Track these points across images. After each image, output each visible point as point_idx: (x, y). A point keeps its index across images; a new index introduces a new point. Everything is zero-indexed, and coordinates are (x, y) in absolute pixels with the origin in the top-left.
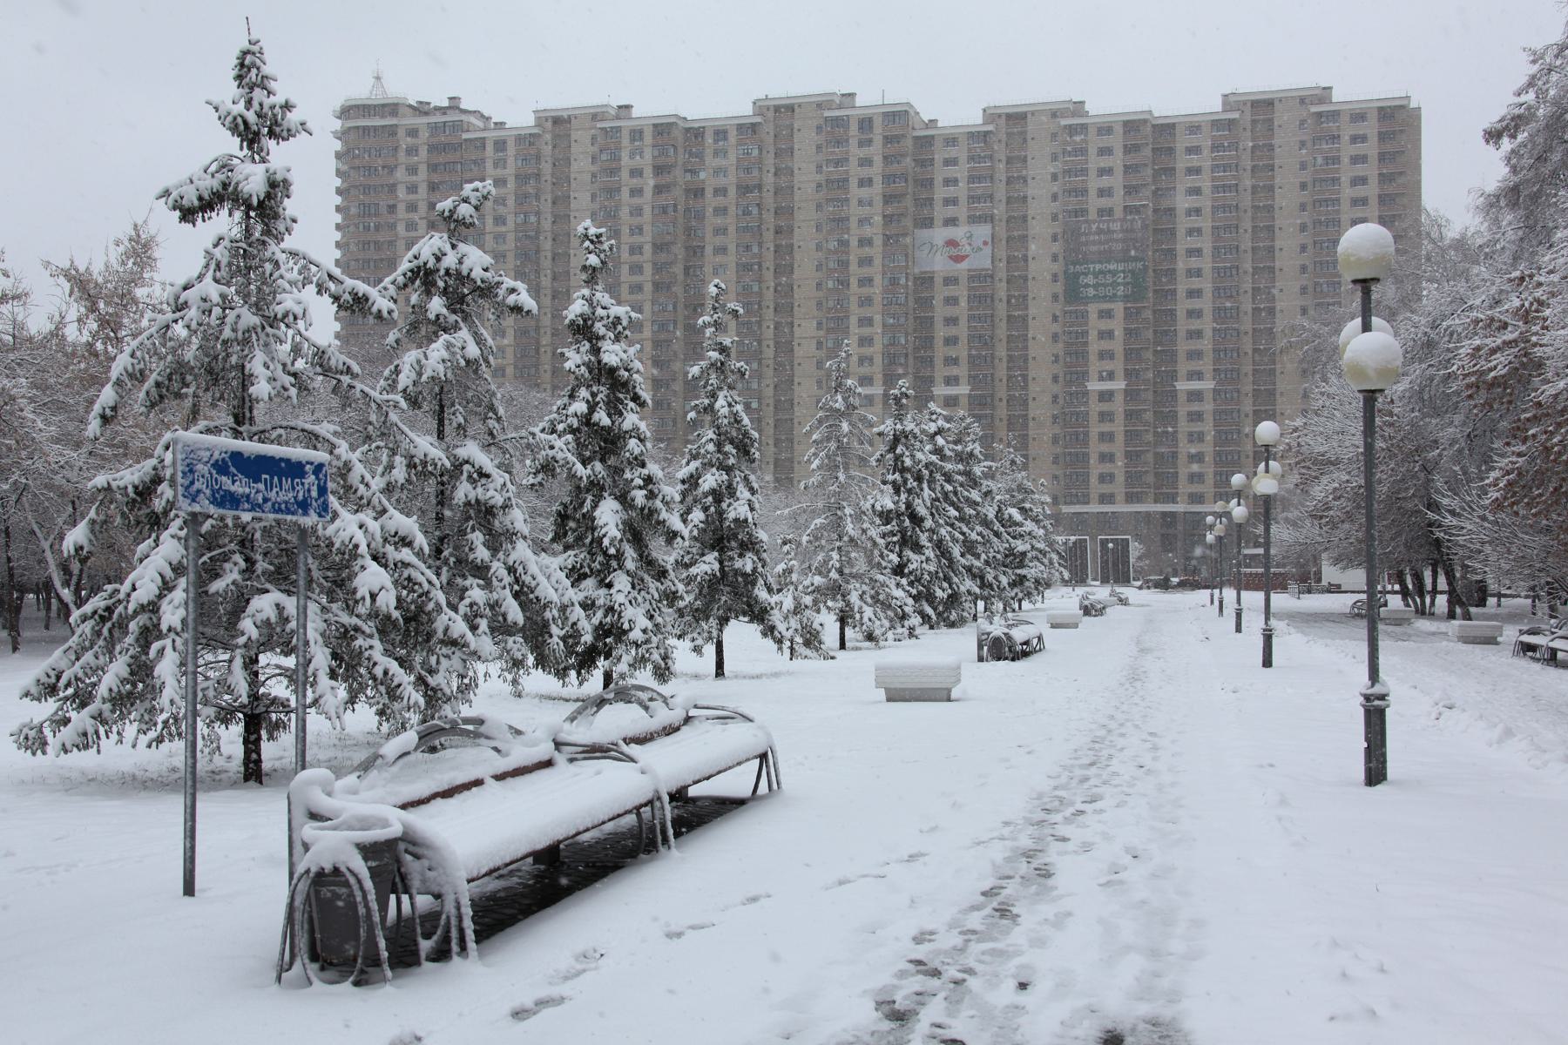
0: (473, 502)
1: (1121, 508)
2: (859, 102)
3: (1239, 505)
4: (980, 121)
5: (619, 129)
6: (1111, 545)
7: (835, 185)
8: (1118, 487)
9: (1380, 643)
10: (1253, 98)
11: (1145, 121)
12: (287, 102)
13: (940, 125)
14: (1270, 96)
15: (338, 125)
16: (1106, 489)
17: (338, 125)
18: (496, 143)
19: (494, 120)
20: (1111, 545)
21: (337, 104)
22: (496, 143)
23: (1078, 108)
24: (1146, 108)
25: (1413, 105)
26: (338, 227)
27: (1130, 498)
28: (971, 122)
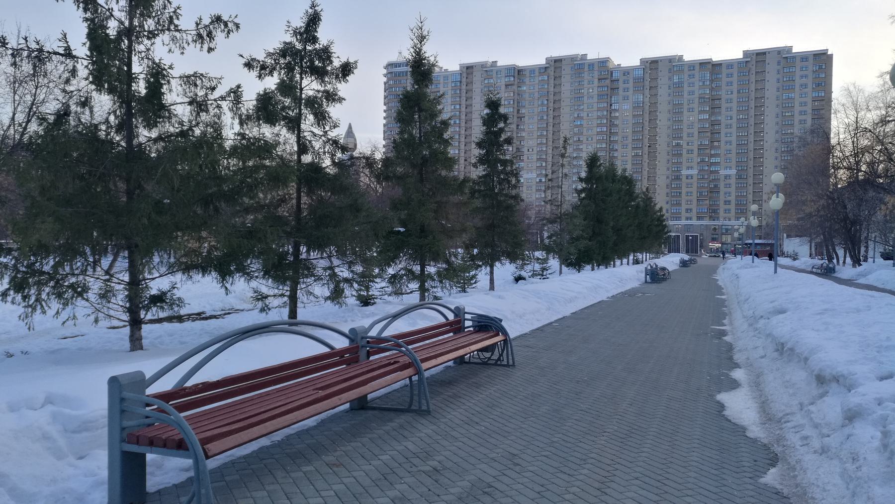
0: (649, 197)
1: (695, 222)
2: (589, 58)
3: (754, 219)
4: (639, 64)
5: (492, 71)
6: (690, 238)
7: (791, 87)
8: (694, 214)
9: (105, 412)
10: (814, 53)
11: (709, 63)
12: (12, 65)
13: (622, 66)
14: (765, 51)
15: (385, 71)
16: (688, 215)
17: (385, 71)
18: (444, 77)
19: (444, 68)
20: (690, 238)
21: (385, 64)
22: (444, 77)
23: (680, 58)
24: (710, 58)
25: (829, 53)
26: (385, 111)
27: (699, 218)
28: (542, 65)
